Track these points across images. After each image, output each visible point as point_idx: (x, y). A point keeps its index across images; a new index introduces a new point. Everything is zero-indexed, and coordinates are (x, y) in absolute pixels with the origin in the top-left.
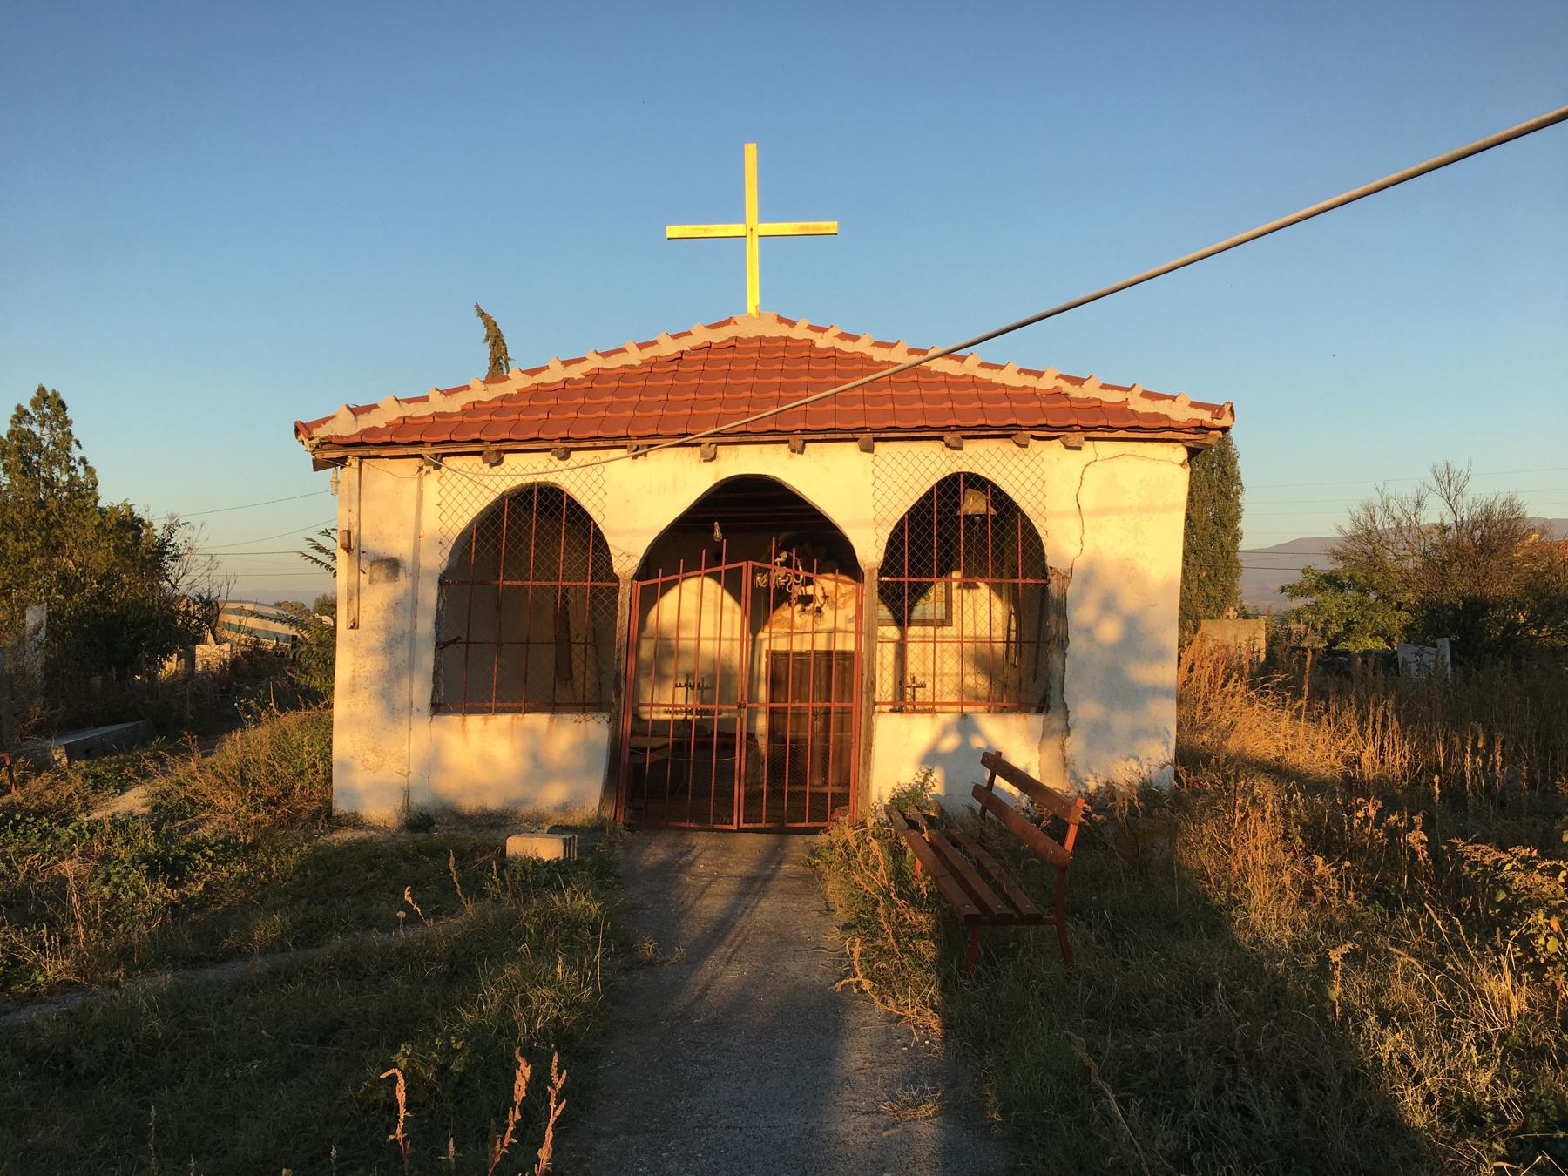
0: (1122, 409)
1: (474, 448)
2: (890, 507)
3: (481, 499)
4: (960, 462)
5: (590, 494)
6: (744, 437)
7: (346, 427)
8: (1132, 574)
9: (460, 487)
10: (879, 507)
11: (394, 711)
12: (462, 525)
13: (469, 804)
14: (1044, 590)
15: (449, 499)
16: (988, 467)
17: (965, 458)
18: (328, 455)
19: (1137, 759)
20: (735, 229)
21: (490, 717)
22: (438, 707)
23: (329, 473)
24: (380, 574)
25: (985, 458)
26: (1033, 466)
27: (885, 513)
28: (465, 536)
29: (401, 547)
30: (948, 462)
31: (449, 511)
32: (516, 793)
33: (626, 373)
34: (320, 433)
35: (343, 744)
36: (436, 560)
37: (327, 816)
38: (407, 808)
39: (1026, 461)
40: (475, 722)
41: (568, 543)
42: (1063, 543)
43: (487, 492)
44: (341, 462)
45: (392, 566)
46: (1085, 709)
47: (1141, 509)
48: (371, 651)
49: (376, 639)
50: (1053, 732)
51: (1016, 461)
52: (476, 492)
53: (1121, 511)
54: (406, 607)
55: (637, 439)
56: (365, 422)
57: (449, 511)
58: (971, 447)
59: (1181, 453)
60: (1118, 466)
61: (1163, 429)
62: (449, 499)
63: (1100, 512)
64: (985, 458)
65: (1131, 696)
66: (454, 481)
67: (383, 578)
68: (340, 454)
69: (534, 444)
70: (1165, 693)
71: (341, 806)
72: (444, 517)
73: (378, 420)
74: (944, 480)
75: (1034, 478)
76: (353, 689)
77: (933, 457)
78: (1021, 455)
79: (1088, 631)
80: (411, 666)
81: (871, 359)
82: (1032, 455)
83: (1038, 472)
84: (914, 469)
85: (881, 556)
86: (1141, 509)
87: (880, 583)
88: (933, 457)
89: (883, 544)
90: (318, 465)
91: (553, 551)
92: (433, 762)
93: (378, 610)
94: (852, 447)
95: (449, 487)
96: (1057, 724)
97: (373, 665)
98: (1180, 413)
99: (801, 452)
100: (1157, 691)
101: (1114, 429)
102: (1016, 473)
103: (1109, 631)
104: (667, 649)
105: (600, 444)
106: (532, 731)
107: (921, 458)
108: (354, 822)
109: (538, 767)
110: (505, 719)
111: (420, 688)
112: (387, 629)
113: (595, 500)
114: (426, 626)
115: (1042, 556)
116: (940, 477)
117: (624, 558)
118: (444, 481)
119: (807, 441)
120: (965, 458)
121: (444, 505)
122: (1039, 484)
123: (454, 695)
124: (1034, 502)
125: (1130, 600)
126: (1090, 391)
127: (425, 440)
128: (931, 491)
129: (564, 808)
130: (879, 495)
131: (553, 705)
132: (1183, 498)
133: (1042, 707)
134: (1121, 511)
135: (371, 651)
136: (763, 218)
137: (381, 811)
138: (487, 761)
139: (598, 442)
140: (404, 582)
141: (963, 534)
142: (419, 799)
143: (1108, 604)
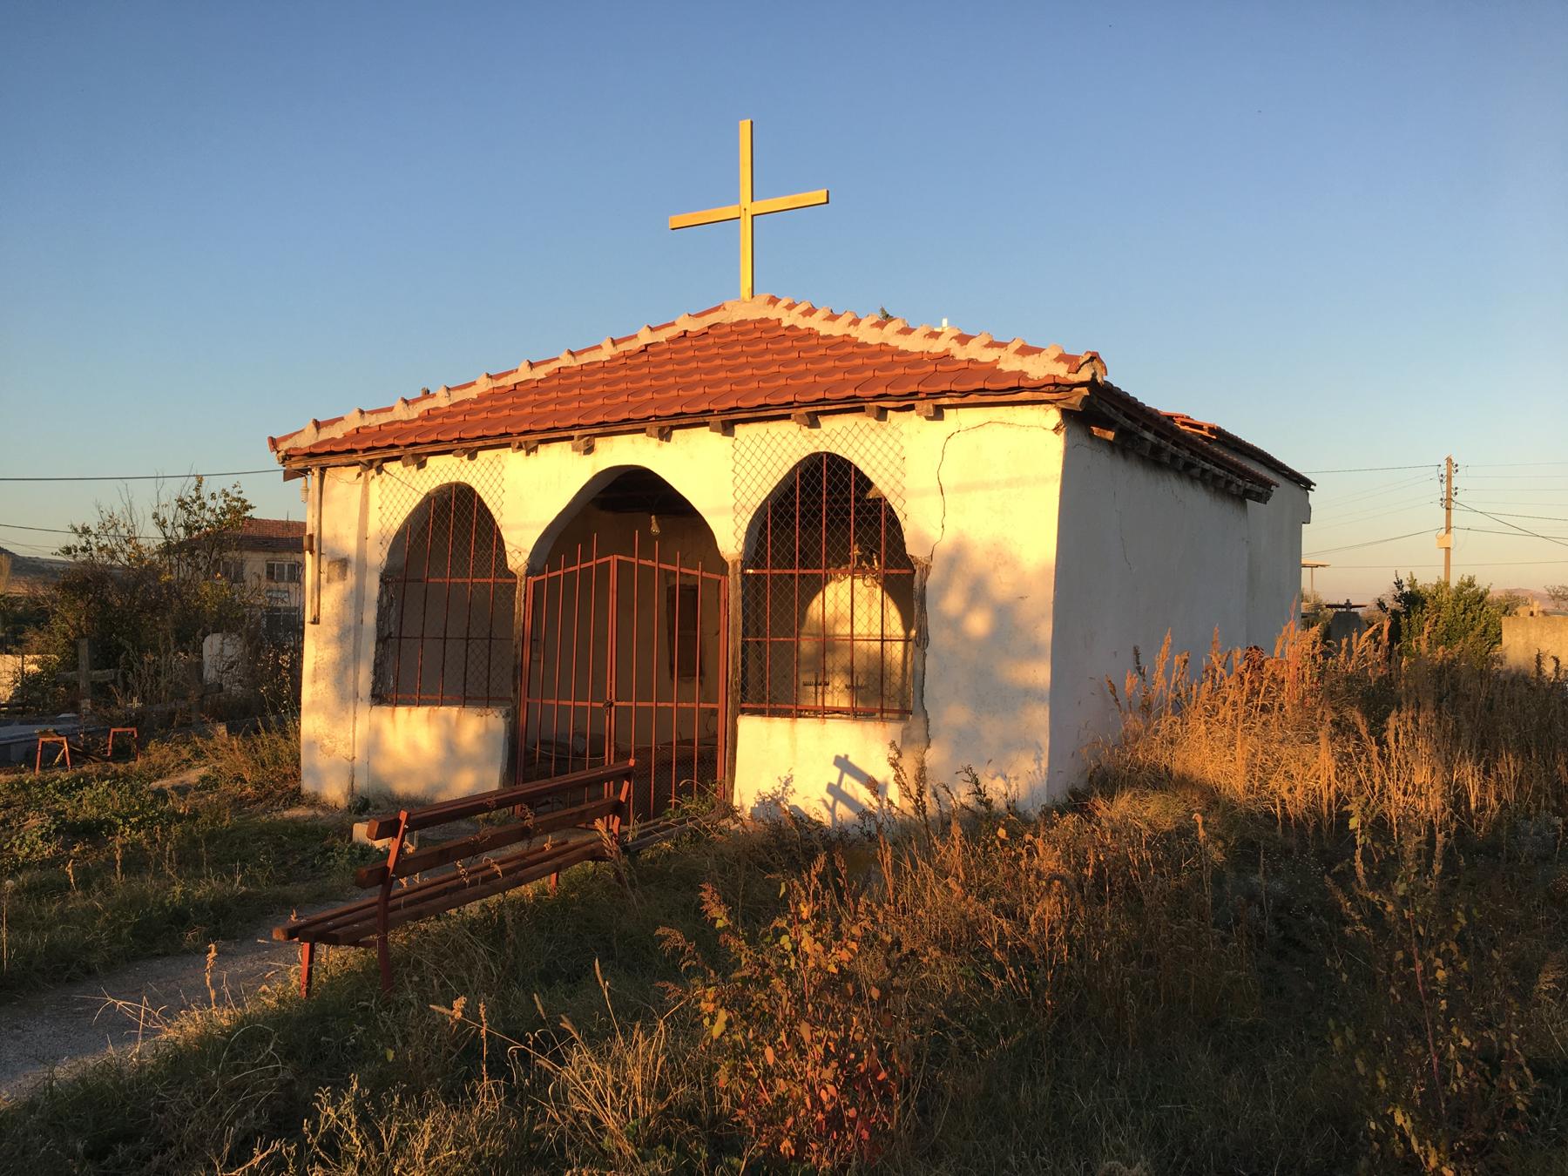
0: (992, 370)
2: (749, 494)
4: (816, 442)
6: (611, 428)
7: (306, 441)
8: (1010, 562)
10: (738, 494)
11: (346, 697)
12: (396, 526)
16: (845, 446)
17: (822, 437)
18: (295, 466)
19: (1005, 777)
20: (731, 212)
21: (414, 709)
22: (381, 697)
23: (300, 481)
25: (844, 436)
26: (891, 442)
27: (744, 500)
28: (400, 535)
30: (805, 442)
33: (603, 367)
34: (284, 446)
36: (378, 556)
37: (296, 797)
39: (884, 436)
40: (402, 711)
42: (925, 523)
44: (303, 472)
45: (343, 563)
47: (1010, 483)
49: (333, 631)
50: (913, 741)
51: (873, 436)
53: (986, 486)
54: (356, 598)
55: (531, 438)
56: (325, 434)
58: (830, 424)
59: (1053, 416)
61: (1019, 389)
63: (963, 488)
64: (844, 436)
65: (995, 697)
68: (301, 465)
70: (1041, 699)
71: (308, 785)
73: (337, 432)
74: (471, 489)
75: (891, 455)
77: (790, 437)
78: (878, 430)
79: (955, 624)
80: (356, 656)
81: (817, 333)
82: (889, 430)
83: (897, 448)
84: (775, 449)
85: (740, 547)
86: (1010, 483)
87: (744, 575)
88: (790, 437)
89: (742, 535)
90: (288, 476)
91: (789, 537)
92: (374, 746)
98: (1037, 368)
99: (668, 440)
100: (1028, 694)
101: (966, 394)
102: (873, 450)
103: (978, 623)
104: (827, 643)
105: (490, 442)
106: (447, 720)
107: (779, 438)
108: (314, 801)
109: (452, 755)
110: (422, 711)
111: (364, 677)
114: (370, 617)
115: (903, 544)
116: (797, 459)
117: (516, 554)
119: (673, 428)
120: (822, 437)
122: (738, 469)
123: (389, 690)
124: (892, 482)
125: (1002, 586)
127: (373, 450)
130: (738, 481)
131: (466, 698)
132: (1057, 469)
133: (904, 713)
134: (986, 486)
136: (736, 200)
138: (414, 747)
139: (501, 441)
140: (351, 579)
141: (830, 515)
142: (361, 783)
143: (978, 592)
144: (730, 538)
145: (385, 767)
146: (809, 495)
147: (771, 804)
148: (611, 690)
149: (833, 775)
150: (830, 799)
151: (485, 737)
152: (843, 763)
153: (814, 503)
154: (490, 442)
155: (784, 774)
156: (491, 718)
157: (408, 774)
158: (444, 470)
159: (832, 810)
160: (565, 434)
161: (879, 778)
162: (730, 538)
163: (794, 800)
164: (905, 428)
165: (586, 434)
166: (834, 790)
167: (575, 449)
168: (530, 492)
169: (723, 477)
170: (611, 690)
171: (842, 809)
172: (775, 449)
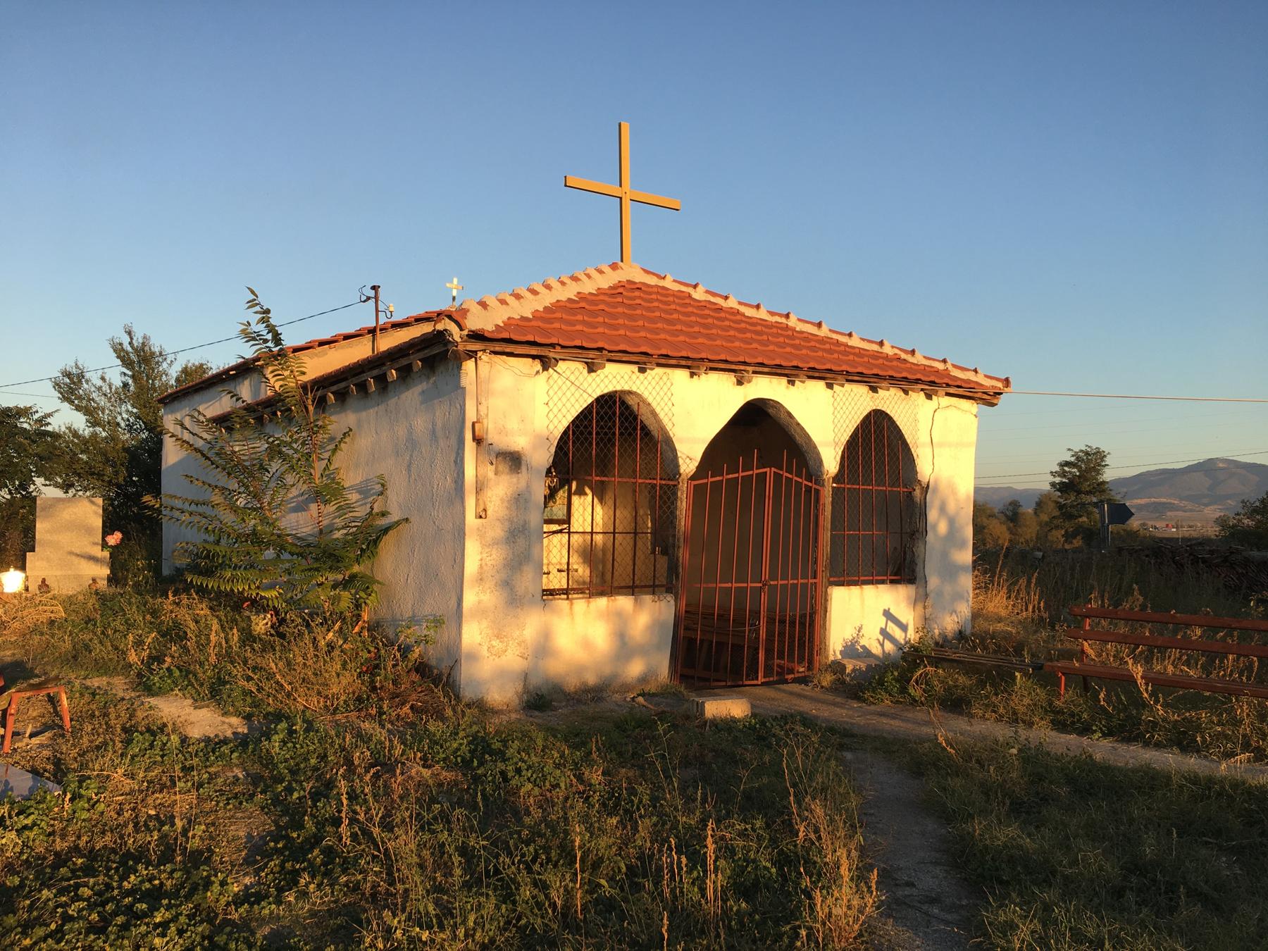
1: (534, 351)
3: (581, 401)
5: (662, 404)
9: (564, 388)
12: (565, 423)
13: (572, 683)
14: (910, 495)
15: (556, 399)
24: (503, 467)
29: (519, 442)
31: (555, 410)
32: (607, 671)
35: (473, 635)
38: (526, 690)
41: (621, 445)
43: (585, 395)
45: (513, 460)
46: (933, 582)
48: (495, 543)
52: (577, 395)
57: (555, 410)
60: (952, 412)
62: (556, 399)
63: (941, 445)
64: (890, 401)
66: (560, 382)
67: (507, 470)
69: (776, 370)
72: (551, 415)
74: (602, 396)
76: (480, 579)
77: (577, 373)
84: (855, 402)
92: (543, 648)
93: (502, 500)
94: (821, 384)
95: (556, 388)
96: (921, 590)
97: (496, 556)
100: (963, 568)
109: (624, 647)
112: (510, 520)
113: (666, 409)
118: (551, 381)
121: (551, 404)
126: (918, 359)
128: (591, 404)
129: (643, 679)
135: (495, 543)
137: (501, 694)
138: (586, 644)
139: (667, 361)
140: (523, 477)
142: (534, 681)
143: (943, 509)
144: (831, 461)
145: (555, 668)
146: (626, 429)
147: (851, 650)
148: (766, 574)
149: (882, 621)
150: (881, 638)
151: (656, 625)
152: (887, 614)
153: (602, 428)
154: (766, 370)
155: (858, 625)
156: (663, 604)
157: (581, 669)
158: (616, 377)
159: (882, 645)
160: (734, 367)
161: (904, 621)
162: (831, 461)
163: (863, 642)
164: (157, 344)
165: (593, 357)
166: (883, 632)
167: (749, 381)
168: (693, 410)
169: (824, 416)
170: (766, 574)
171: (889, 646)
172: (855, 402)
